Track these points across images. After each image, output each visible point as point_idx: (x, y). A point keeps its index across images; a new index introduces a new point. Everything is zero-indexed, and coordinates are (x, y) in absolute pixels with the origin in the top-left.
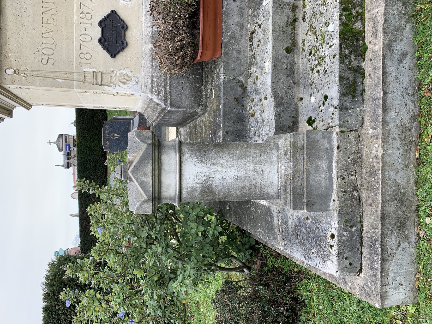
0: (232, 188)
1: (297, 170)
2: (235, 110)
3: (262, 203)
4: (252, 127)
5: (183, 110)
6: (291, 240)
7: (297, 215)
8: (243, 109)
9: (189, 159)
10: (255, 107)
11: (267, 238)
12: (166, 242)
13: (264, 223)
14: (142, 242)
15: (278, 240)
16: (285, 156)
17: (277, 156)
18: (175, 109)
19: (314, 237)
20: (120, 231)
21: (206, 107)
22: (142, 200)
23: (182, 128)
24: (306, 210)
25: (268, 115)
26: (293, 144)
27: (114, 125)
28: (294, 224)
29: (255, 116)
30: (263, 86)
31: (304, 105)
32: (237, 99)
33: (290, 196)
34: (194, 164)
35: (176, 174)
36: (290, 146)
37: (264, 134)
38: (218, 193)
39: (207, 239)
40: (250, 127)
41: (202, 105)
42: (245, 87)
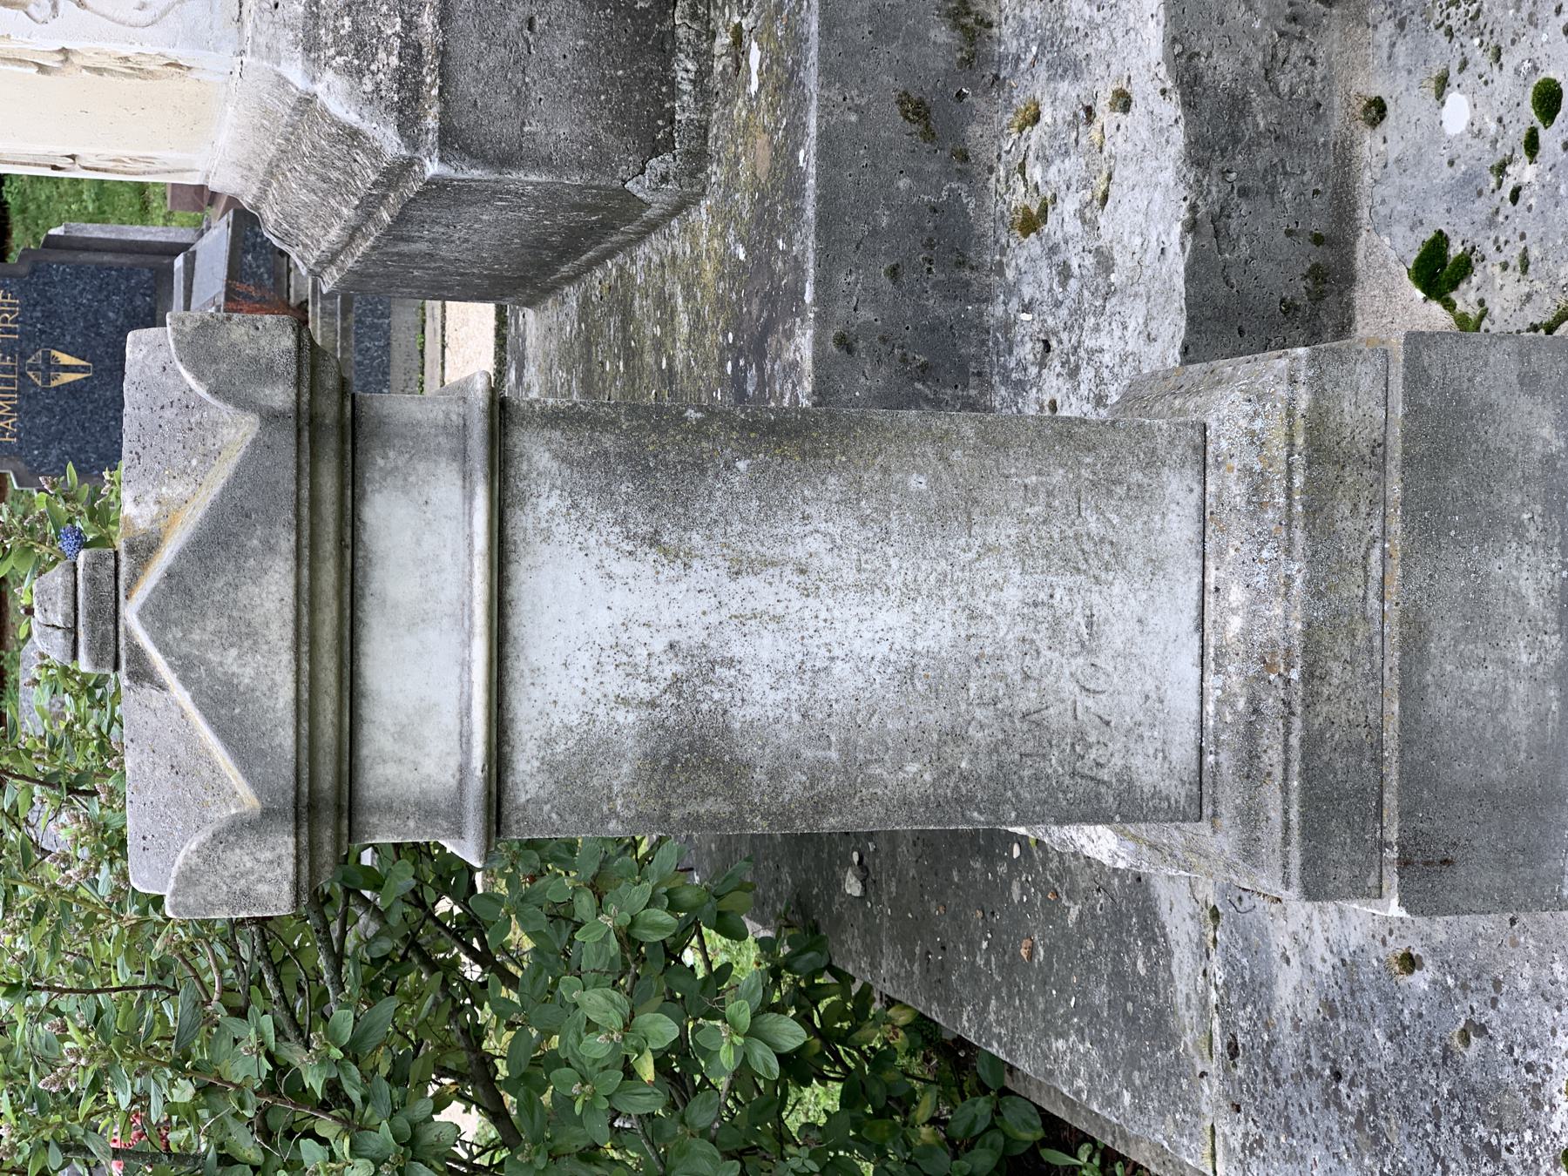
0: (872, 741)
1: (1338, 614)
2: (903, 183)
3: (1089, 850)
4: (1027, 308)
5: (533, 178)
6: (1294, 1111)
7: (1333, 935)
8: (963, 175)
9: (564, 528)
10: (1047, 162)
11: (1127, 1097)
12: (402, 1122)
13: (1100, 995)
14: (230, 1120)
15: (1197, 1113)
16: (1252, 515)
17: (1193, 512)
18: (476, 173)
19: (1452, 1095)
20: (76, 1041)
21: (698, 158)
22: (225, 813)
23: (530, 314)
24: (1395, 901)
25: (1140, 218)
26: (1309, 430)
27: (51, 292)
28: (1312, 1001)
29: (1046, 229)
30: (1106, 12)
31: (1394, 150)
32: (921, 102)
33: (1286, 801)
34: (595, 560)
35: (470, 635)
36: (1291, 445)
37: (1106, 358)
38: (773, 775)
39: (696, 1104)
40: (1014, 304)
41: (668, 145)
42: (980, 22)
